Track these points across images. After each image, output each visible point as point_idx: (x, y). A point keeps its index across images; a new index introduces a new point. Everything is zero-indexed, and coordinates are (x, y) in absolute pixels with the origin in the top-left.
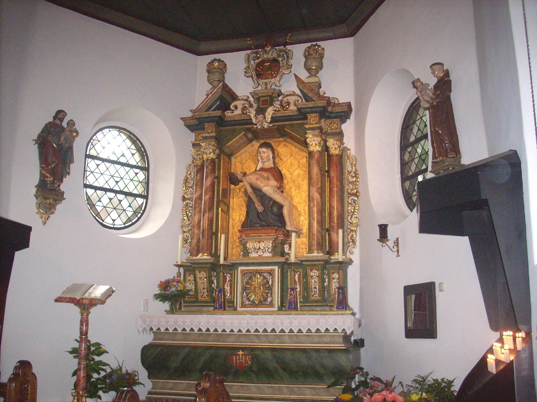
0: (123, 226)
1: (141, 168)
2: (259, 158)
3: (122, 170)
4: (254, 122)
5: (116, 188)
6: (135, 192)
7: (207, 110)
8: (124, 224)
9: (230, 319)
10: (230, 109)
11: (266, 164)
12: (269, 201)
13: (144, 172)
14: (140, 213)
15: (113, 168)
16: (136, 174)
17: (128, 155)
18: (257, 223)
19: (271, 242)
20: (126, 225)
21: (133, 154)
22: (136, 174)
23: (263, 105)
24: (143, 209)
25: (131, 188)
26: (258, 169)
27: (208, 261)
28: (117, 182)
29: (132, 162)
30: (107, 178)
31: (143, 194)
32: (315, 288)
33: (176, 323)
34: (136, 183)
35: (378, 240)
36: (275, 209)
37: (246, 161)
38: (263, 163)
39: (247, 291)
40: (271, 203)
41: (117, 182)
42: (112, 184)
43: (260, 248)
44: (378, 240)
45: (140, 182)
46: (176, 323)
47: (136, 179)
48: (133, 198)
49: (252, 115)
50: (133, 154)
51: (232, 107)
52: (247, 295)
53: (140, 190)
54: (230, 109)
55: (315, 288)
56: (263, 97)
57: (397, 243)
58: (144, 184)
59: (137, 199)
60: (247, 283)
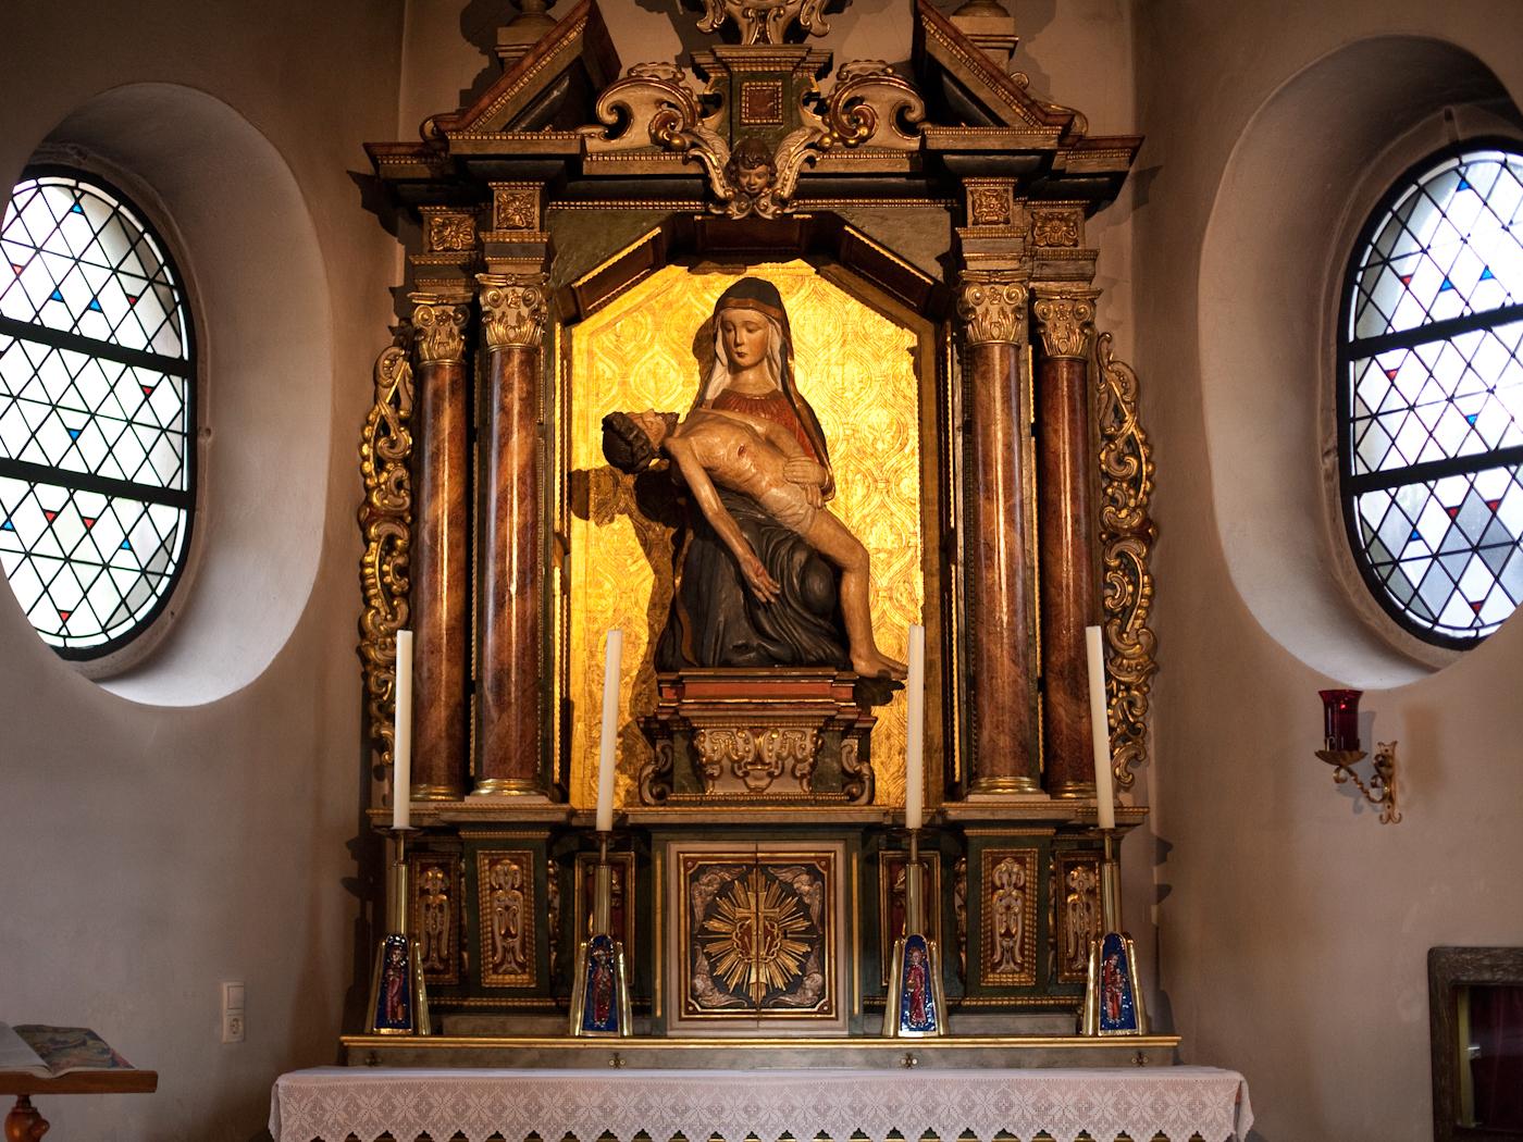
0: (102, 639)
1: (164, 365)
2: (720, 349)
3: (96, 376)
4: (720, 192)
5: (73, 464)
6: (146, 478)
7: (508, 128)
8: (105, 630)
9: (1188, 1086)
10: (594, 120)
11: (750, 376)
12: (793, 549)
13: (177, 380)
14: (163, 575)
15: (58, 366)
16: (148, 391)
17: (114, 301)
18: (745, 648)
19: (810, 732)
20: (114, 634)
21: (133, 300)
22: (148, 391)
23: (753, 115)
24: (176, 556)
25: (127, 463)
26: (710, 395)
27: (545, 818)
28: (75, 434)
29: (131, 338)
30: (36, 413)
31: (175, 486)
32: (1008, 934)
33: (1085, 1109)
34: (148, 436)
35: (1320, 755)
36: (818, 586)
37: (642, 349)
38: (735, 368)
39: (713, 948)
40: (800, 557)
41: (75, 434)
42: (52, 448)
43: (759, 759)
44: (1320, 755)
45: (164, 431)
46: (1085, 1109)
47: (72, 400)
48: (23, 486)
49: (712, 160)
50: (133, 300)
51: (603, 110)
52: (713, 967)
53: (164, 468)
54: (594, 120)
55: (1008, 934)
56: (753, 76)
57: (1384, 765)
58: (177, 440)
59: (117, 502)
60: (712, 911)
